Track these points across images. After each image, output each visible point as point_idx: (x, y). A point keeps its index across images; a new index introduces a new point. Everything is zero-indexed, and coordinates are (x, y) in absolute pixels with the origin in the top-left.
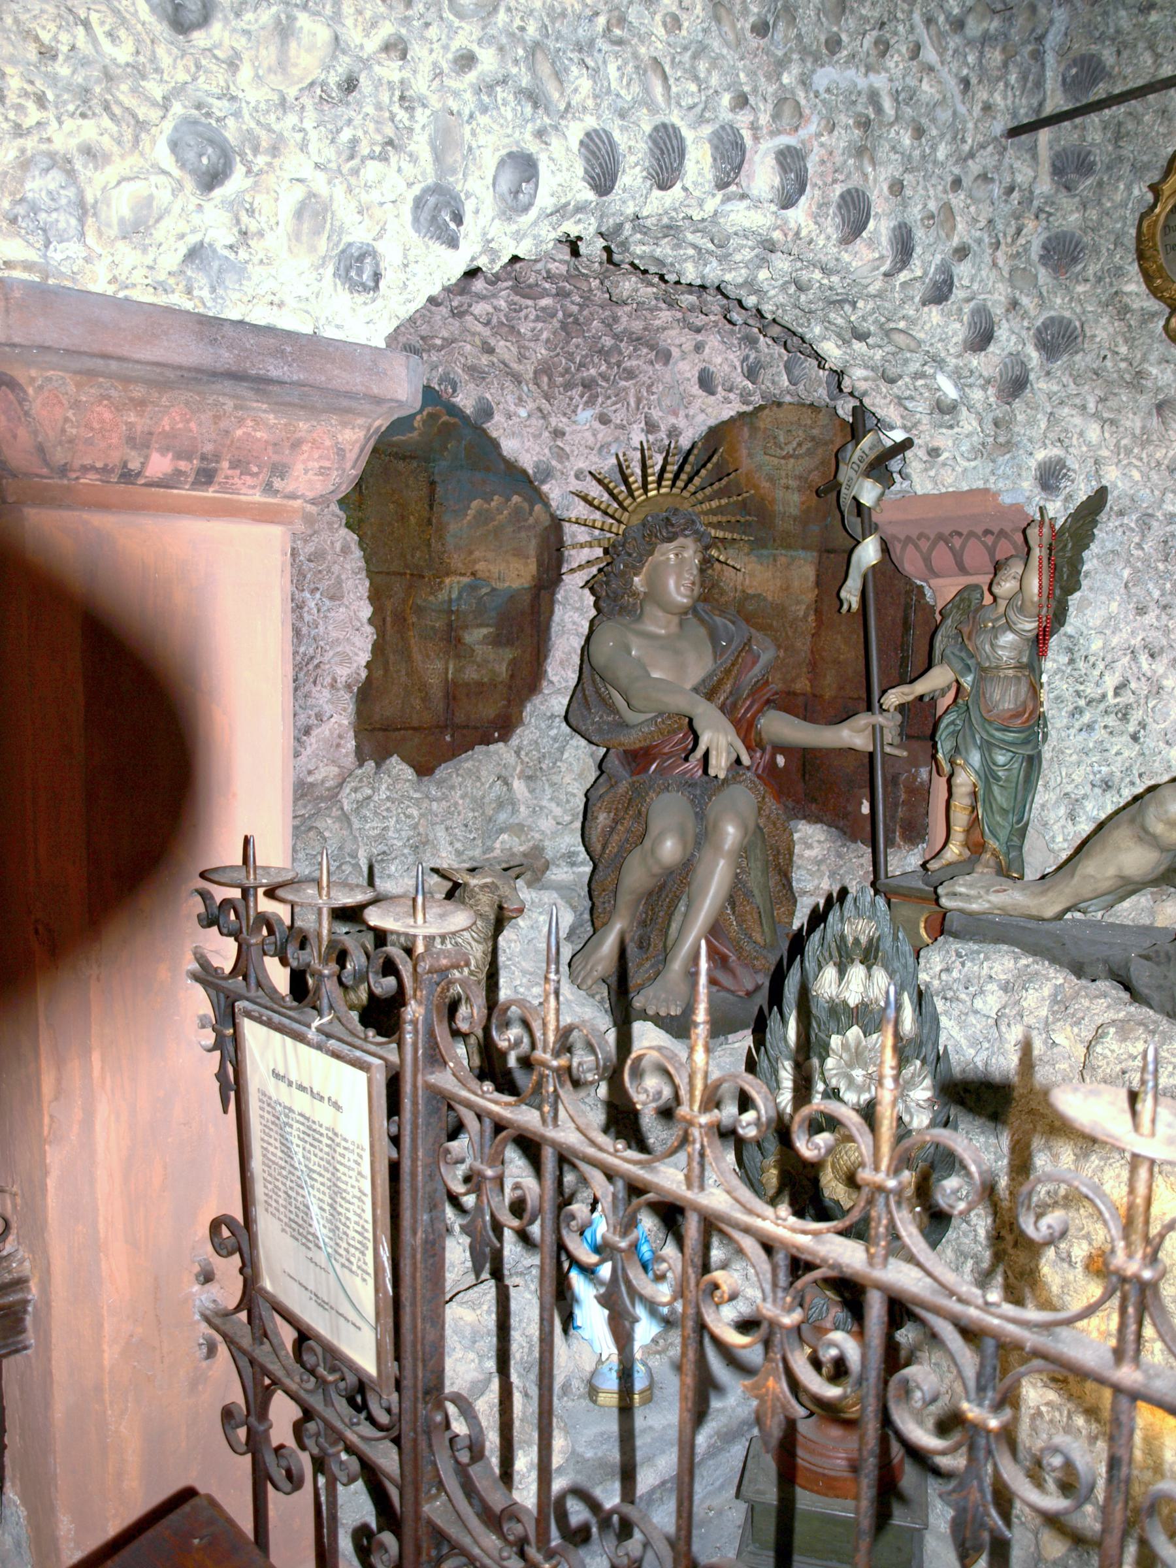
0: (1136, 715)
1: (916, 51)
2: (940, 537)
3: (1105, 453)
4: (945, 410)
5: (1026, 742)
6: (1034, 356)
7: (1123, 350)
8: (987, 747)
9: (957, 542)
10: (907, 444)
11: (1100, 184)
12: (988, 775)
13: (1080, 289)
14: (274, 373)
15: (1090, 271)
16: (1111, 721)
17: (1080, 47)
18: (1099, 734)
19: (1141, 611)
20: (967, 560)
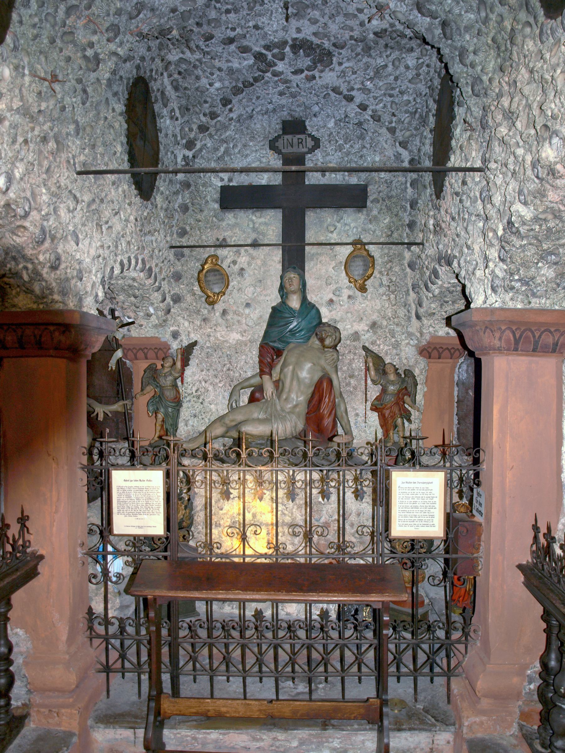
0: (202, 397)
2: (140, 349)
3: (190, 330)
4: (149, 315)
5: (177, 406)
7: (195, 304)
8: (166, 407)
9: (146, 351)
10: (133, 323)
12: (166, 414)
13: (182, 286)
16: (195, 399)
17: (181, 225)
18: (192, 403)
19: (202, 371)
20: (149, 356)
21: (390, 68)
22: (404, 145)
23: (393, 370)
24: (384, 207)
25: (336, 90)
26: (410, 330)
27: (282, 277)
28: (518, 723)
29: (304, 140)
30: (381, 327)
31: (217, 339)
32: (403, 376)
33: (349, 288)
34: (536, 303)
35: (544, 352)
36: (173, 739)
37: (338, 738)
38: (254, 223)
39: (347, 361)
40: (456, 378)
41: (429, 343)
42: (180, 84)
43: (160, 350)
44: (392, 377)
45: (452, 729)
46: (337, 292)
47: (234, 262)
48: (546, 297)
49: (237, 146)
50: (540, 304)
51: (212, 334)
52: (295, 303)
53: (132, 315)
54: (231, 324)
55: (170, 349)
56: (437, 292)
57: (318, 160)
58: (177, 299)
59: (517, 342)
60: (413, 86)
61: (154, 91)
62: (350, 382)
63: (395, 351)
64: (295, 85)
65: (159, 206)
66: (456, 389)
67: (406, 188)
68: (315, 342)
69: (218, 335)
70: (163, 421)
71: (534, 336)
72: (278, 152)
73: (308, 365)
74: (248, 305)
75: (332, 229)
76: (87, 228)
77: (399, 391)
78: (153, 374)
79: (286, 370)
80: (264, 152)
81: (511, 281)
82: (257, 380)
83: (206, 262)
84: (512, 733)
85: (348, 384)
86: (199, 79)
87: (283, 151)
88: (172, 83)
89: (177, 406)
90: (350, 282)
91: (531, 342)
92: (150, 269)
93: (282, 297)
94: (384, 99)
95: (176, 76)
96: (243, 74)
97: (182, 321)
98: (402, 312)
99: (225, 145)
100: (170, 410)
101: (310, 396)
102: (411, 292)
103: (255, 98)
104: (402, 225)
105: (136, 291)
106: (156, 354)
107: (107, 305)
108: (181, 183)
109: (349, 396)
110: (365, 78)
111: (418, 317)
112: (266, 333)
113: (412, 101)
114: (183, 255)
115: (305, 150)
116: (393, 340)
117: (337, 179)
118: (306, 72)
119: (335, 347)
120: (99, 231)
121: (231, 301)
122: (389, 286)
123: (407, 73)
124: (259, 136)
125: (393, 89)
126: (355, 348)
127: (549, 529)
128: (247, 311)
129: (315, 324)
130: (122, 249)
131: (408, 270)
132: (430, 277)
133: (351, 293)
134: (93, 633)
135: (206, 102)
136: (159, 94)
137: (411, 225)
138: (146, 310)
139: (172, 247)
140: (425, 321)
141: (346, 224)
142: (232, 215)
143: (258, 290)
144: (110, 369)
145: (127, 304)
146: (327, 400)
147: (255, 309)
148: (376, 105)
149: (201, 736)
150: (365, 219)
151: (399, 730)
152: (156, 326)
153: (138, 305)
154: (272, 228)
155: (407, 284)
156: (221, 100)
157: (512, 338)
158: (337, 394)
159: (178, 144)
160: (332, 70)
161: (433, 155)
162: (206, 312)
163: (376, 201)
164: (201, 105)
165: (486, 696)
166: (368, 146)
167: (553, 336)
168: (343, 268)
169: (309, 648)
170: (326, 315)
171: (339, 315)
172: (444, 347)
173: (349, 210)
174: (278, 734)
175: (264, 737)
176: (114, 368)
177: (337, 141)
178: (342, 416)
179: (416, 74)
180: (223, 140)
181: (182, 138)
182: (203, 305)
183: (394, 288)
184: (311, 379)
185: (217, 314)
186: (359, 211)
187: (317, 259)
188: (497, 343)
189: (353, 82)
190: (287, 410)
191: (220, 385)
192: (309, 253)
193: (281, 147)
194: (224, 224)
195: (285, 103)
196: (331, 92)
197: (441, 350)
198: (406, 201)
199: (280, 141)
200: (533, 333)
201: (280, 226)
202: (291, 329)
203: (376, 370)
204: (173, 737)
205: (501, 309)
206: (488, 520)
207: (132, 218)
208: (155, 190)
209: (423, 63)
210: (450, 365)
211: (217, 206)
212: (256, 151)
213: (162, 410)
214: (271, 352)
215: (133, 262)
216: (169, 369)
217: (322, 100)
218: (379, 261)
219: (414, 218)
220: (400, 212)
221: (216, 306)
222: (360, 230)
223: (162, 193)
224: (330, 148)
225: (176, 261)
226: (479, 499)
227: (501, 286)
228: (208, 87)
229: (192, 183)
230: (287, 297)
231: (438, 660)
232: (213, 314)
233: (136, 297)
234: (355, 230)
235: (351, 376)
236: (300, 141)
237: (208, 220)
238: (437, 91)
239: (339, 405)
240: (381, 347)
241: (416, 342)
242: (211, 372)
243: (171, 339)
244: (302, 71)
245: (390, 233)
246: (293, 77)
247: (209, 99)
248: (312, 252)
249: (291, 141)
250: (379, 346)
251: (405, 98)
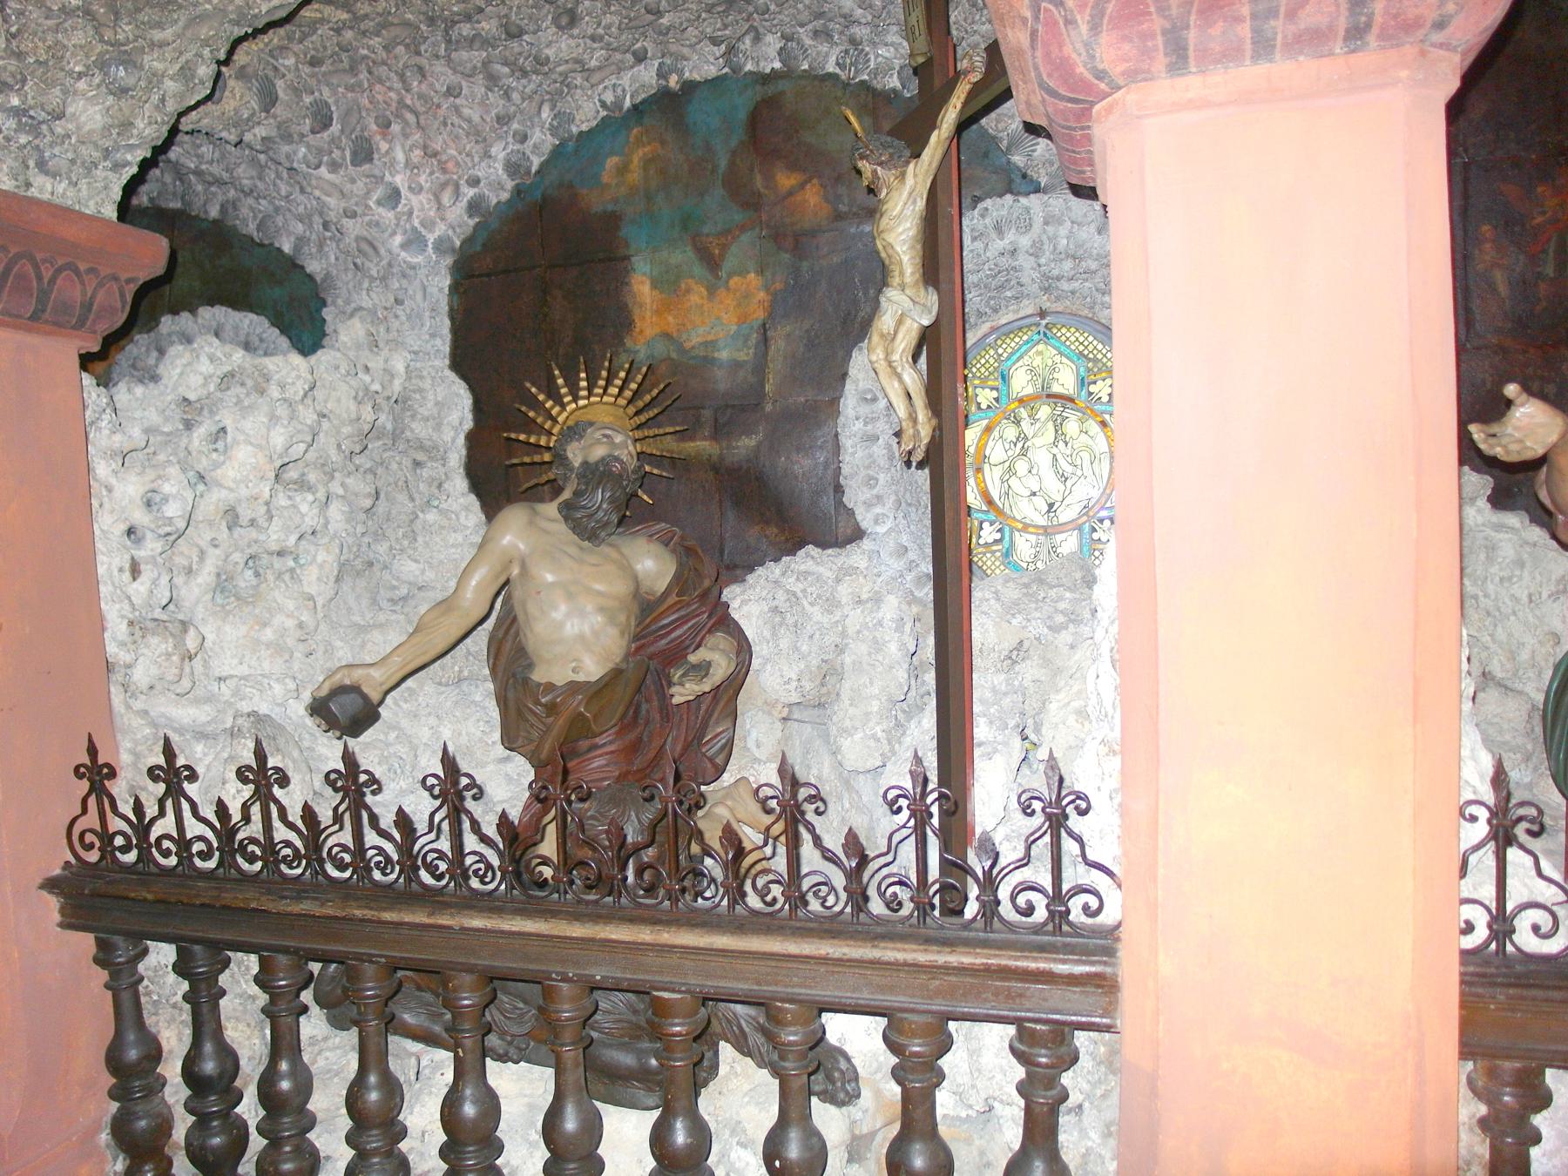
34: (43, 188)
48: (69, 178)
71: (39, 278)
167: (82, 283)
200: (36, 267)
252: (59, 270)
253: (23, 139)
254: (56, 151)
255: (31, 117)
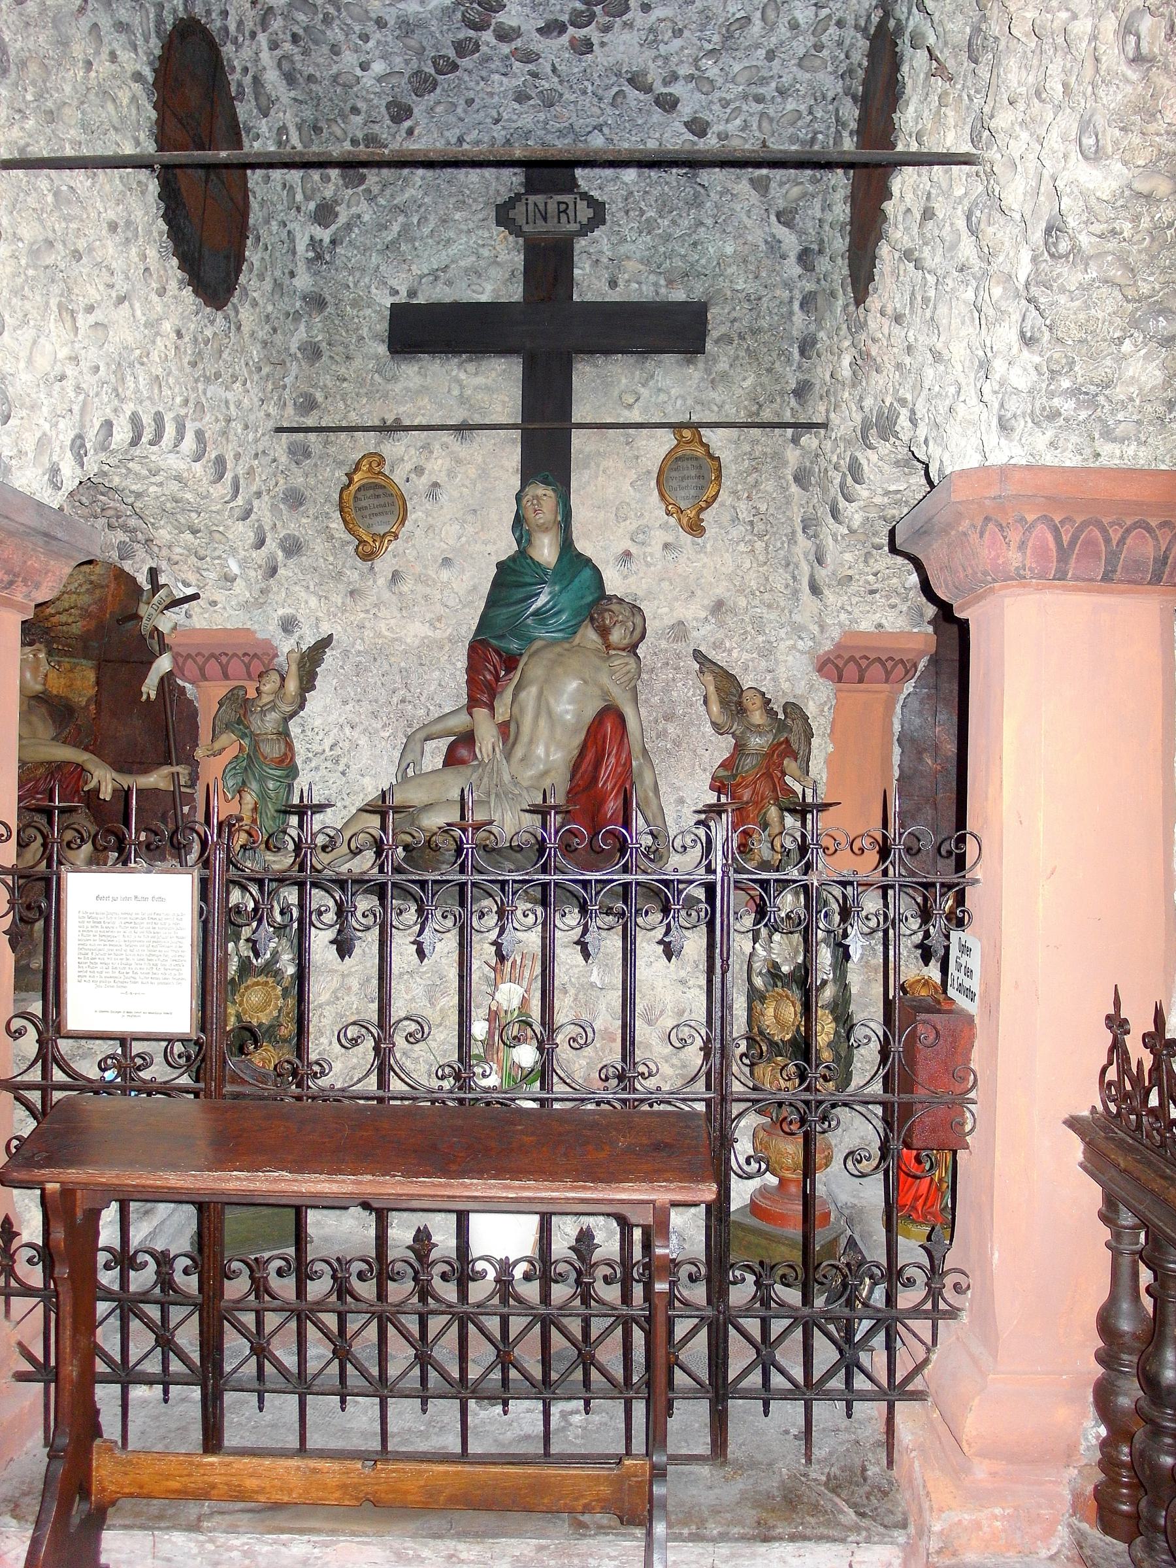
0: (343, 761)
1: (244, 384)
2: (212, 655)
4: (229, 579)
5: (287, 776)
6: (280, 554)
7: (331, 559)
8: (262, 780)
9: (224, 659)
10: (195, 597)
11: (316, 465)
13: (304, 520)
14: (59, 536)
15: (311, 512)
16: (329, 764)
17: (304, 388)
19: (345, 703)
21: (757, 27)
22: (786, 217)
23: (758, 701)
24: (742, 354)
25: (636, 81)
26: (797, 618)
27: (519, 498)
28: (1070, 1526)
29: (571, 206)
30: (733, 611)
31: (379, 635)
32: (781, 716)
33: (664, 527)
34: (1112, 455)
35: (1129, 582)
36: (194, 1557)
37: (611, 1558)
38: (462, 387)
39: (658, 686)
40: (897, 727)
41: (838, 646)
42: (298, 66)
43: (256, 659)
44: (757, 717)
45: (900, 1537)
46: (639, 535)
47: (419, 470)
48: (1138, 439)
49: (426, 219)
50: (1121, 457)
51: (367, 624)
52: (546, 551)
53: (192, 577)
54: (410, 603)
55: (276, 655)
56: (857, 520)
57: (601, 252)
58: (292, 547)
59: (1064, 554)
60: (808, 76)
61: (233, 69)
62: (665, 730)
63: (763, 664)
64: (549, 69)
65: (245, 329)
66: (897, 750)
67: (791, 313)
68: (590, 635)
69: (382, 626)
70: (255, 809)
71: (1108, 541)
72: (516, 231)
73: (573, 685)
74: (447, 562)
75: (631, 401)
76: (28, 305)
77: (774, 748)
78: (239, 709)
79: (523, 695)
80: (486, 235)
81: (1051, 395)
82: (460, 722)
83: (357, 468)
84: (1054, 1550)
85: (662, 735)
86: (337, 54)
87: (526, 228)
88: (279, 65)
89: (287, 776)
90: (668, 513)
91: (1098, 554)
92: (220, 462)
93: (519, 542)
94: (745, 107)
95: (288, 46)
96: (432, 34)
97: (303, 595)
98: (780, 579)
99: (401, 219)
100: (271, 785)
101: (576, 752)
102: (800, 536)
103: (462, 102)
104: (782, 393)
105: (194, 515)
106: (247, 666)
107: (143, 561)
108: (304, 298)
109: (663, 760)
110: (701, 48)
111: (815, 589)
112: (484, 623)
113: (805, 113)
114: (307, 454)
115: (574, 227)
116: (761, 639)
117: (641, 293)
118: (571, 30)
119: (632, 648)
120: (69, 324)
121: (411, 554)
122: (751, 523)
123: (795, 44)
124: (475, 200)
125: (763, 81)
126: (679, 656)
127: (1159, 1018)
128: (445, 575)
129: (589, 599)
130: (137, 391)
131: (794, 489)
132: (842, 486)
133: (670, 539)
134: (13, 1283)
135: (355, 110)
136: (248, 80)
137: (802, 391)
138: (223, 566)
139: (280, 430)
140: (829, 596)
141: (660, 390)
142: (416, 368)
143: (470, 529)
144: (144, 697)
145: (178, 550)
146: (613, 760)
147: (463, 571)
148: (727, 121)
149: (266, 1549)
150: (703, 379)
151: (766, 1539)
152: (245, 606)
153: (202, 552)
154: (501, 397)
155: (791, 519)
156: (388, 106)
157: (1052, 545)
158: (636, 749)
159: (298, 209)
160: (628, 25)
161: (852, 223)
162: (355, 576)
163: (726, 339)
164: (344, 117)
165: (983, 1455)
166: (709, 222)
168: (653, 483)
169: (547, 1323)
170: (614, 582)
171: (644, 586)
172: (872, 656)
173: (669, 359)
174: (461, 1546)
175: (426, 1553)
176: (153, 696)
177: (642, 212)
178: (646, 797)
179: (815, 46)
180: (396, 206)
181: (307, 198)
182: (350, 562)
183: (763, 527)
184: (578, 715)
185: (381, 581)
186: (689, 362)
187: (598, 466)
188: (1014, 558)
189: (675, 59)
190: (525, 784)
191: (383, 734)
192: (581, 452)
193: (521, 220)
194: (398, 388)
195: (530, 126)
196: (627, 88)
197: (864, 663)
198: (791, 339)
199: (520, 208)
201: (518, 393)
202: (536, 609)
203: (724, 704)
204: (195, 1551)
205: (1029, 467)
206: (991, 1009)
207: (167, 327)
208: (237, 293)
209: (829, 16)
210: (883, 696)
211: (382, 349)
212: (469, 232)
213: (254, 785)
214: (493, 660)
215: (170, 430)
216: (271, 698)
217: (609, 110)
218: (730, 470)
219: (806, 377)
220: (777, 365)
221: (378, 564)
222: (690, 402)
223: (255, 304)
224: (628, 227)
225: (293, 465)
226: (964, 960)
227: (1024, 414)
228: (359, 72)
229: (328, 298)
230: (529, 541)
231: (864, 1358)
232: (371, 582)
233: (194, 532)
234: (679, 402)
235: (668, 718)
236: (563, 207)
237: (364, 380)
238: (861, 74)
239: (640, 775)
240: (735, 654)
241: (811, 643)
242: (366, 707)
243: (280, 634)
244: (562, 28)
245: (755, 408)
246: (540, 44)
247: (362, 105)
248: (587, 449)
249: (542, 207)
250: (730, 651)
251: (791, 105)
252: (1128, 531)
253: (1083, 414)
254: (1120, 416)
255: (1087, 393)
